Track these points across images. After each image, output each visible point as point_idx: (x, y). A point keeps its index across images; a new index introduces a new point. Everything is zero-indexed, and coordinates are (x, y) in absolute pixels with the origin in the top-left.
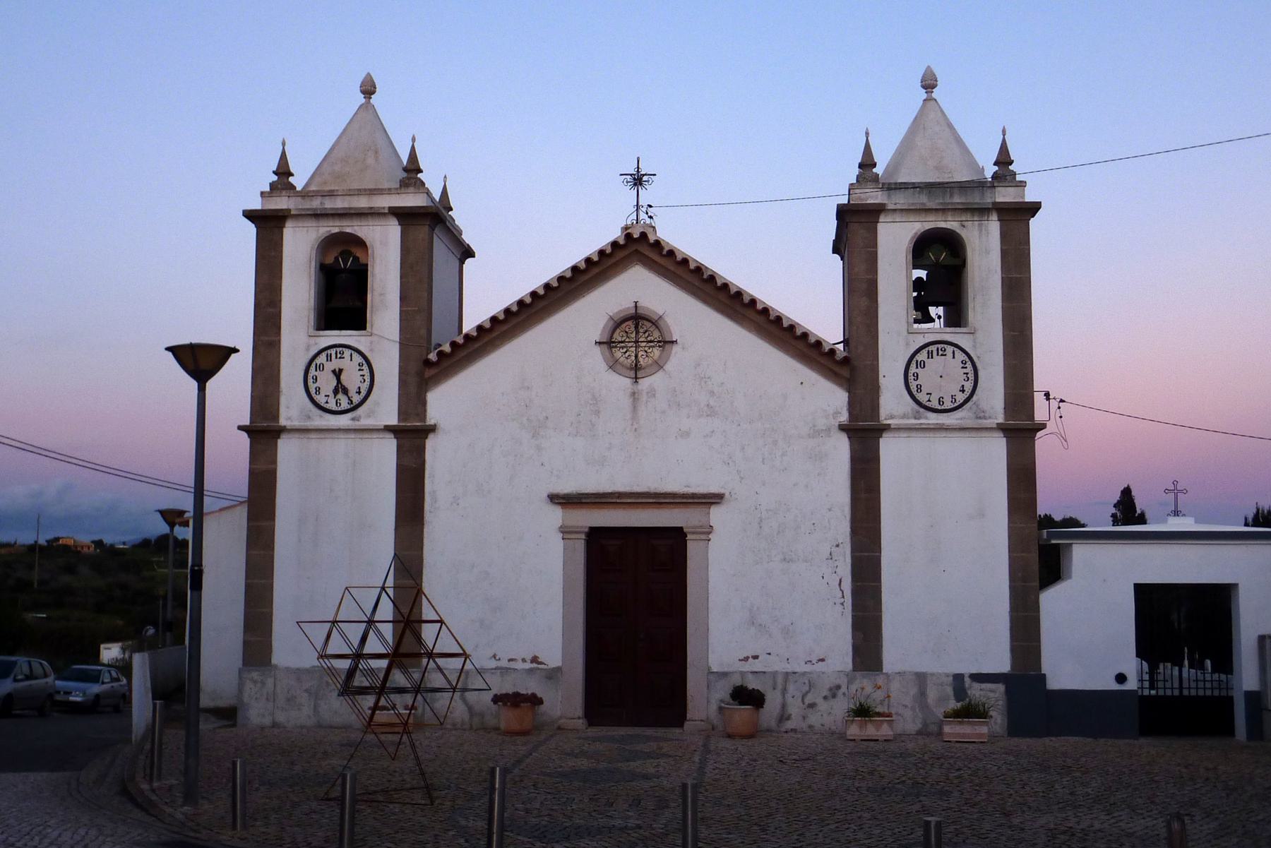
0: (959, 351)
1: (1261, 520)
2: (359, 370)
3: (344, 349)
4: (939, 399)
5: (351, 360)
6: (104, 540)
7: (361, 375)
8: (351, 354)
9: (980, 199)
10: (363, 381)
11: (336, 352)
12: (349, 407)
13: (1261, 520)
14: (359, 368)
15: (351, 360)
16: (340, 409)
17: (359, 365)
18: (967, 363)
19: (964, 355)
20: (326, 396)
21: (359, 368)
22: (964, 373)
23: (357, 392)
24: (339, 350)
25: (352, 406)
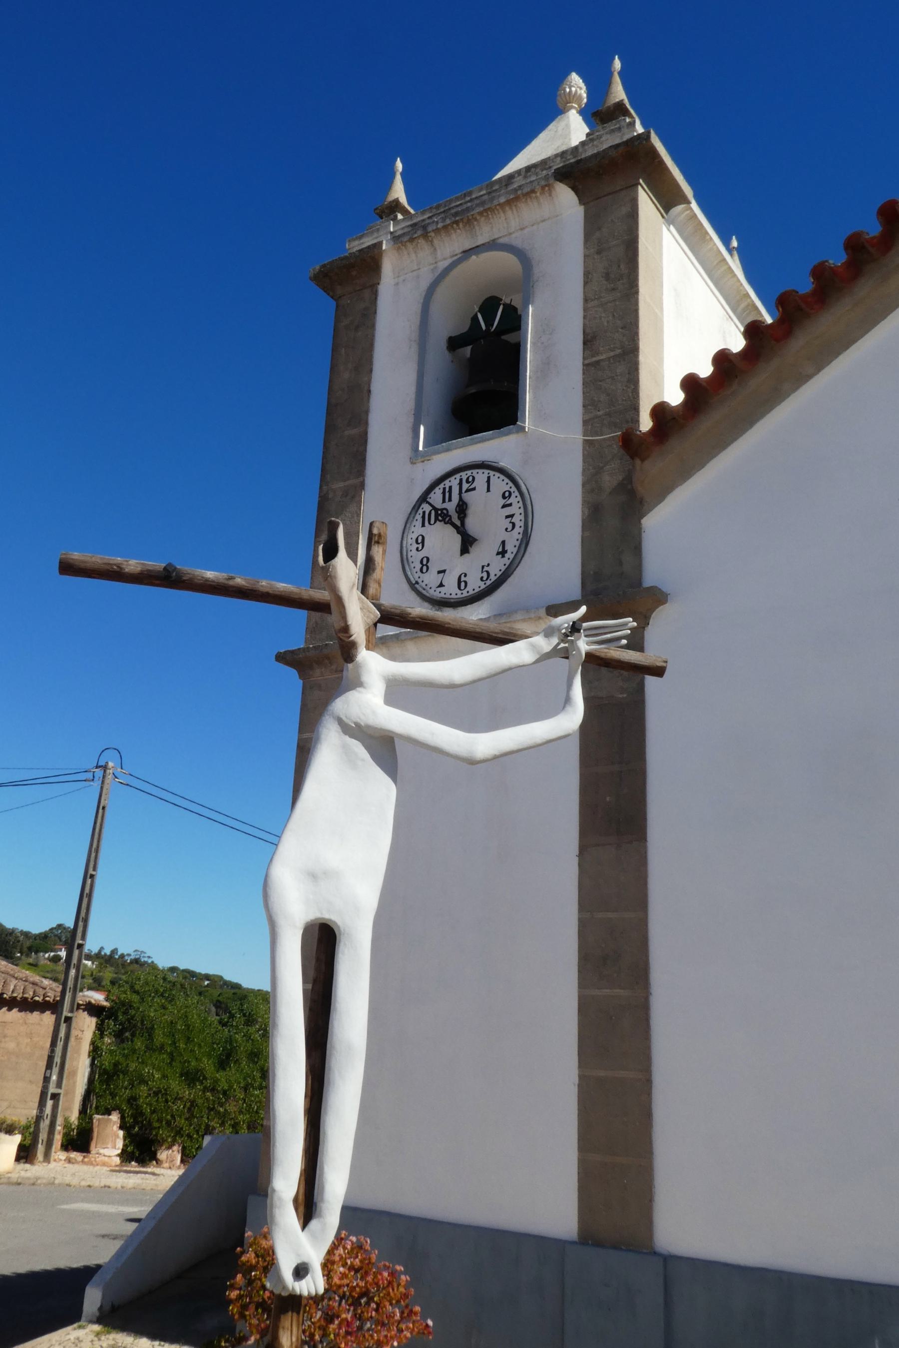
0: (497, 474)
1: (625, 695)
2: (504, 506)
3: (475, 471)
4: (460, 577)
5: (488, 490)
6: (30, 1014)
7: (507, 517)
8: (489, 478)
9: (626, 113)
10: (510, 527)
11: (461, 480)
12: (483, 587)
13: (625, 695)
14: (502, 502)
15: (488, 490)
16: (465, 594)
17: (504, 497)
18: (513, 496)
19: (507, 480)
20: (439, 572)
21: (502, 502)
22: (507, 517)
23: (498, 554)
24: (464, 475)
25: (489, 582)
